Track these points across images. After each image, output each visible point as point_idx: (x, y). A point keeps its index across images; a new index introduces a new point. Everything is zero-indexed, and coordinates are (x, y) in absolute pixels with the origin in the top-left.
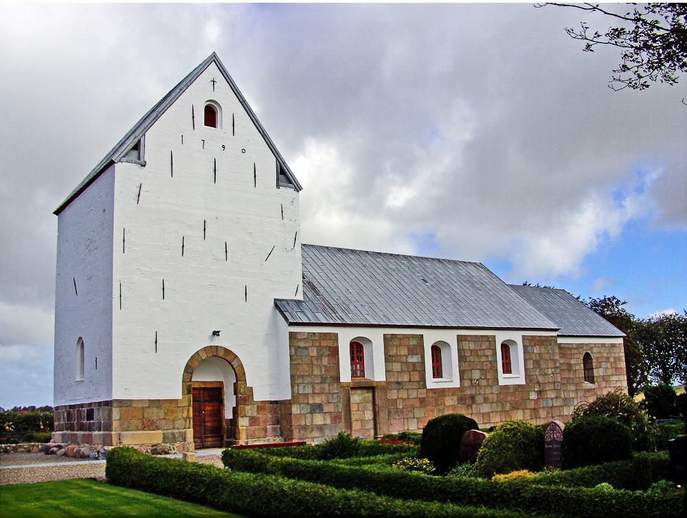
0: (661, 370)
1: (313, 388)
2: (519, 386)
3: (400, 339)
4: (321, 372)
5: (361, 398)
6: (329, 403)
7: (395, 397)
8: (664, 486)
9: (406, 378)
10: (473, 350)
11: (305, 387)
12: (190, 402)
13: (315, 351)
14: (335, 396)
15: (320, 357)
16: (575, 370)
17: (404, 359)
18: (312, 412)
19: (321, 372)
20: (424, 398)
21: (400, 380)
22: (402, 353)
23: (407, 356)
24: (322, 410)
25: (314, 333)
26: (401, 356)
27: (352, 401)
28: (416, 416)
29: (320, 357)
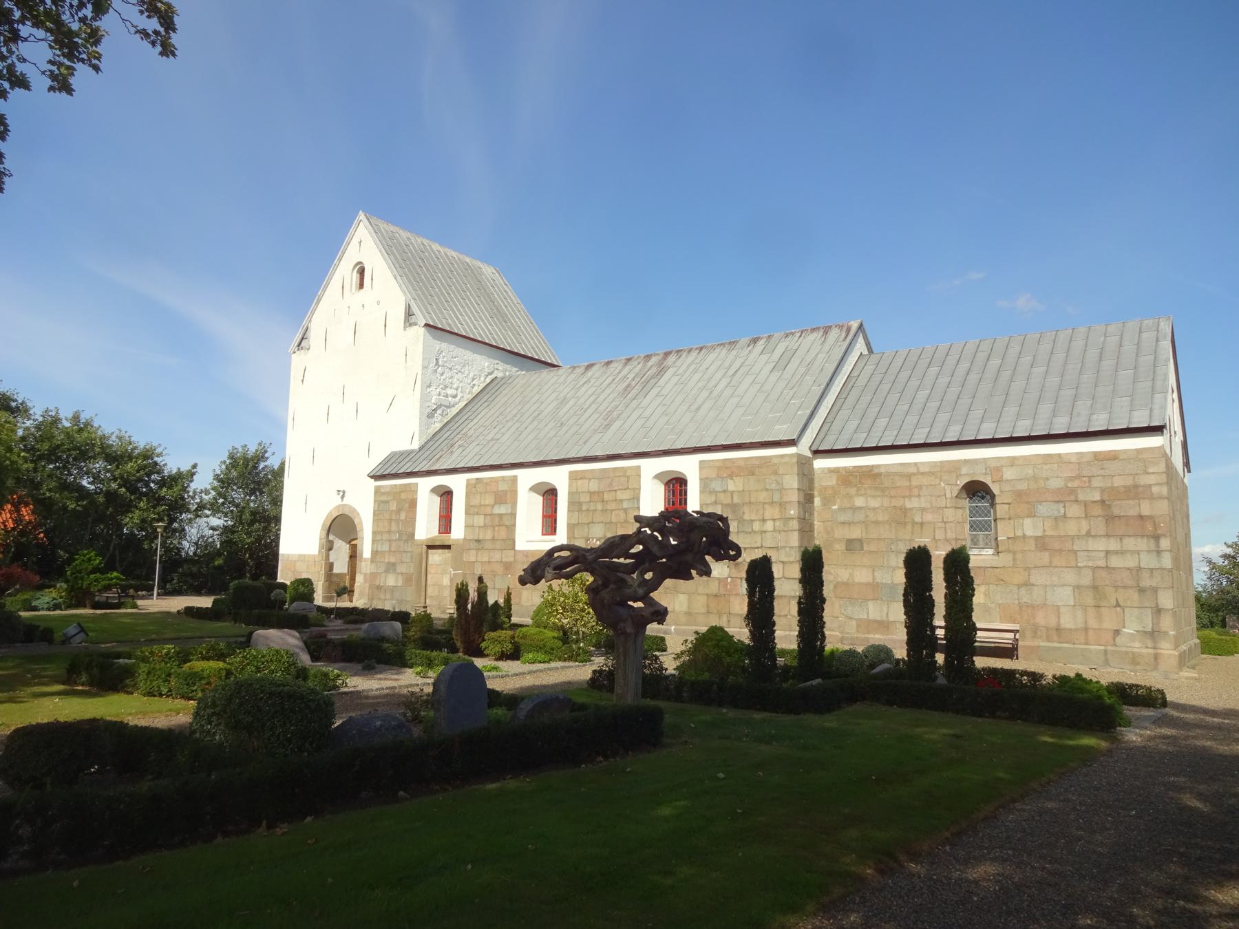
0: (123, 490)
1: (390, 546)
2: (511, 528)
3: (487, 484)
4: (398, 527)
5: (441, 558)
6: (402, 562)
7: (473, 559)
8: (19, 419)
9: (489, 535)
10: (594, 492)
11: (383, 543)
12: (322, 567)
13: (395, 506)
14: (409, 555)
15: (399, 511)
16: (922, 524)
17: (488, 510)
18: (387, 571)
19: (398, 527)
20: (510, 563)
21: (481, 538)
22: (487, 503)
23: (493, 506)
24: (395, 570)
25: (396, 485)
26: (485, 506)
27: (430, 562)
28: (497, 587)
29: (399, 511)
